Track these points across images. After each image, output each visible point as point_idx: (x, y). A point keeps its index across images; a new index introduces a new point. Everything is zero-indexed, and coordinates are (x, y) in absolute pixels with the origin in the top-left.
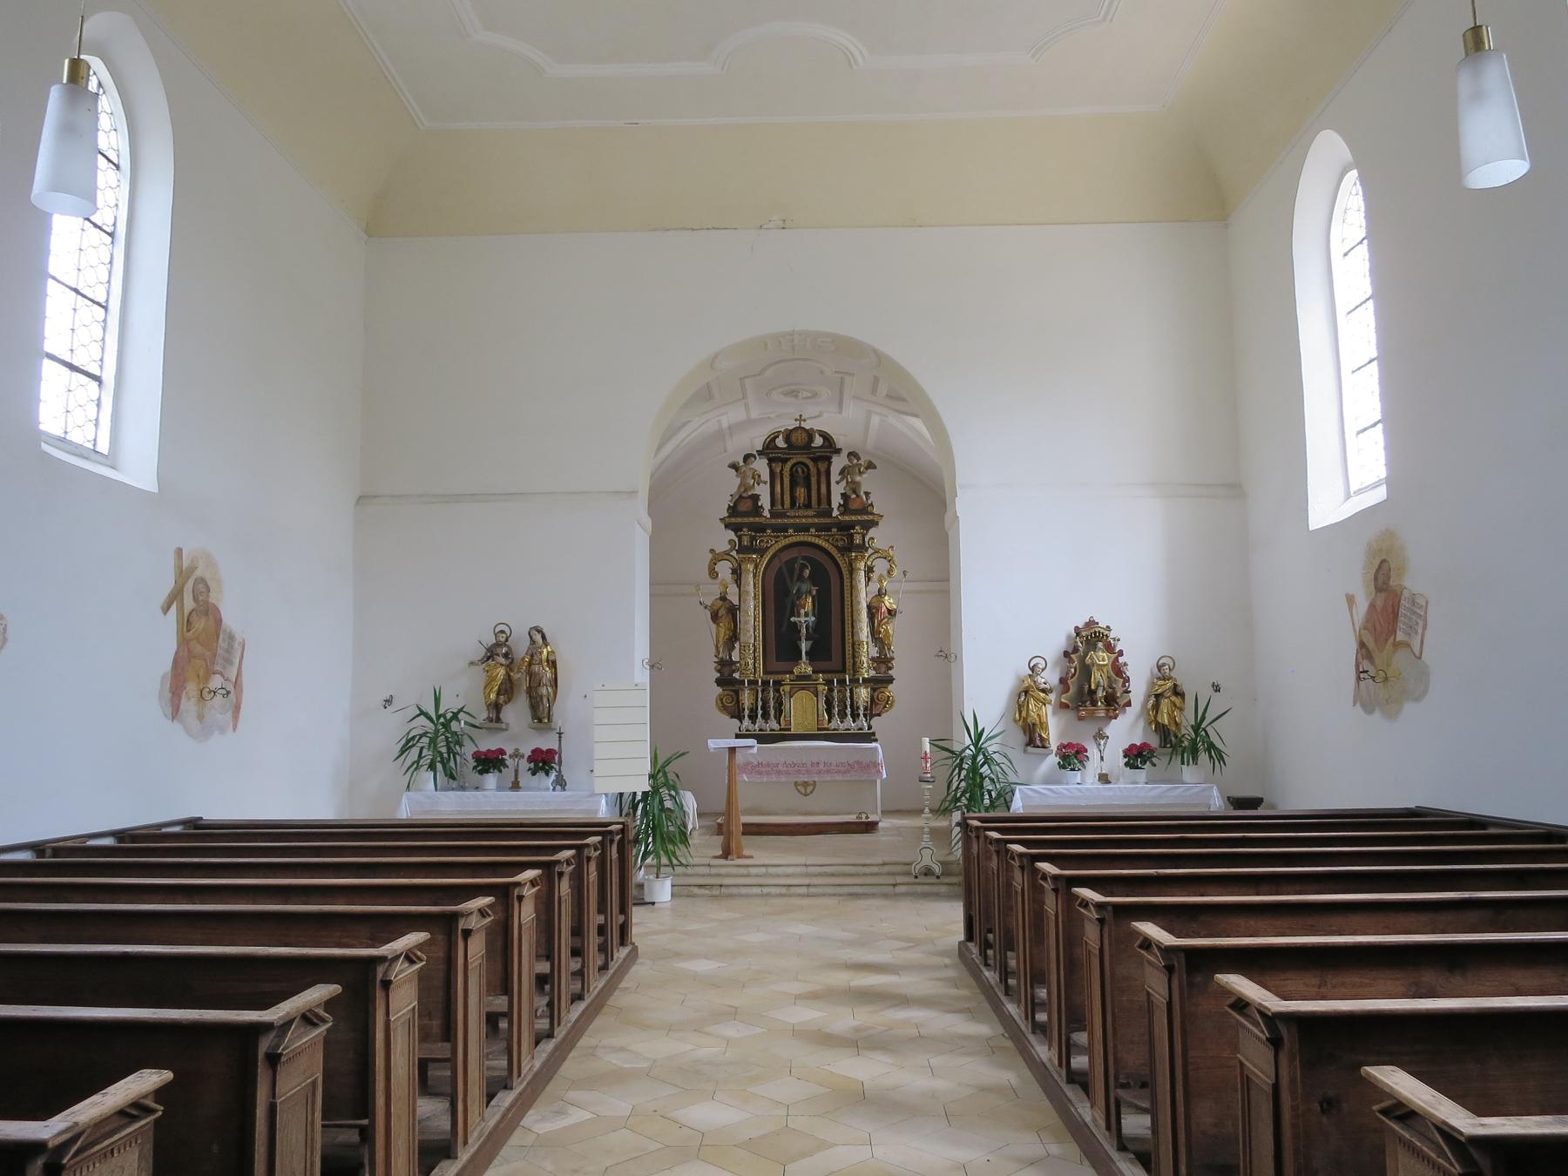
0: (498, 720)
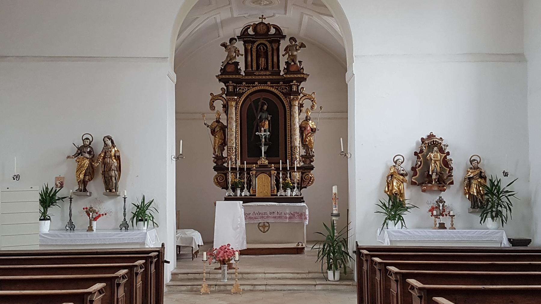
0: (85, 190)
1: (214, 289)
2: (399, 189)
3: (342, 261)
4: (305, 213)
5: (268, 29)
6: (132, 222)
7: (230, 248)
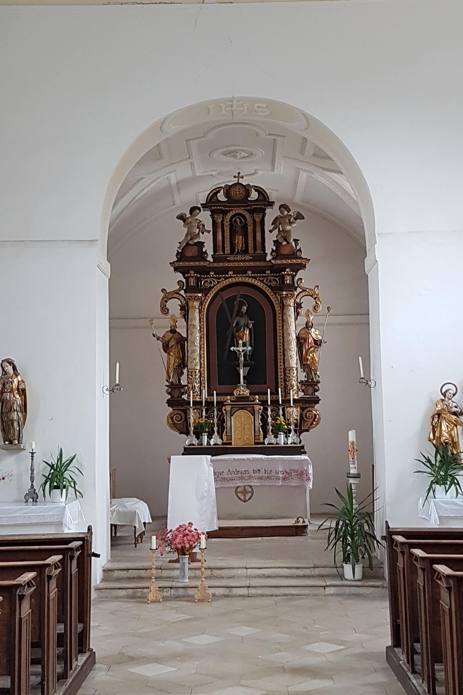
1: (168, 594)
2: (451, 435)
3: (366, 549)
4: (307, 471)
5: (248, 193)
6: (44, 490)
7: (192, 529)
